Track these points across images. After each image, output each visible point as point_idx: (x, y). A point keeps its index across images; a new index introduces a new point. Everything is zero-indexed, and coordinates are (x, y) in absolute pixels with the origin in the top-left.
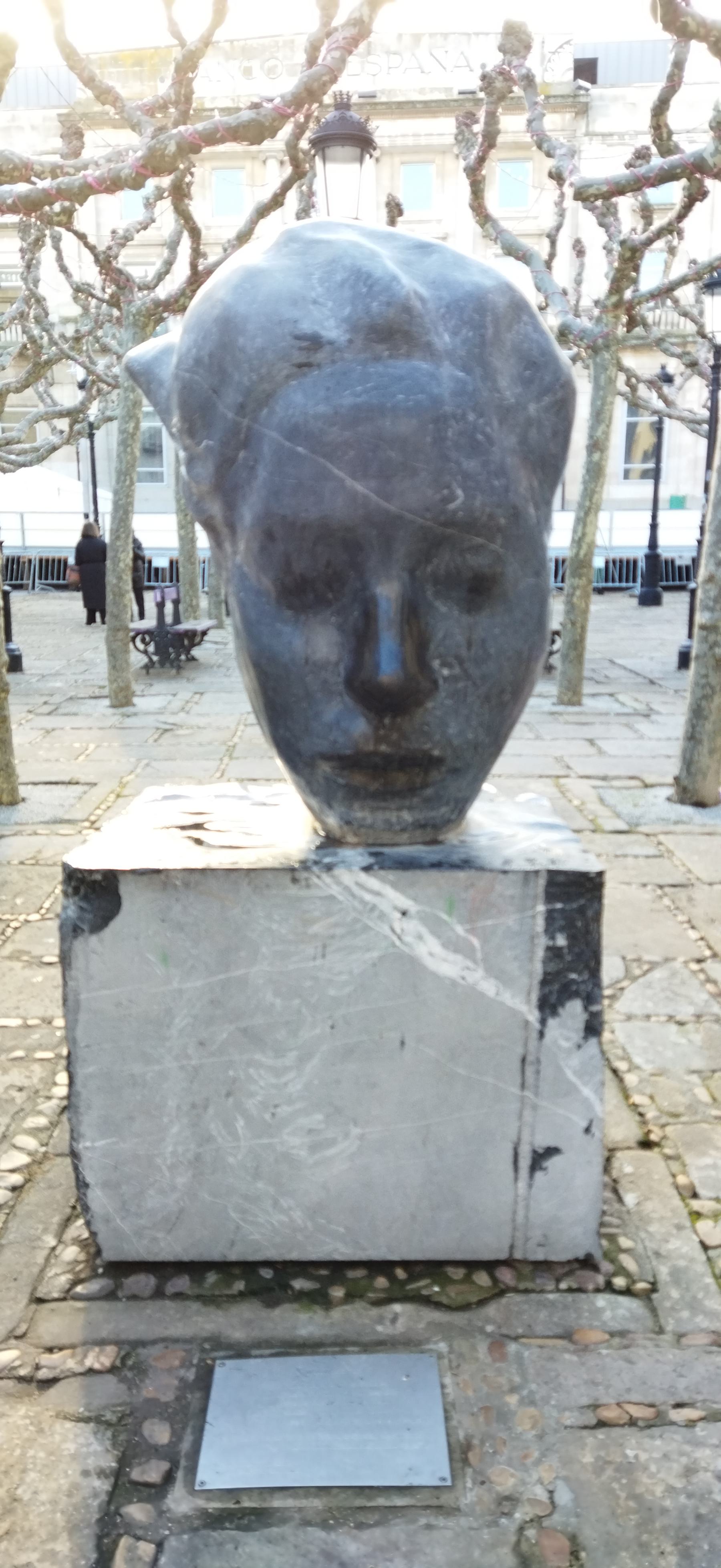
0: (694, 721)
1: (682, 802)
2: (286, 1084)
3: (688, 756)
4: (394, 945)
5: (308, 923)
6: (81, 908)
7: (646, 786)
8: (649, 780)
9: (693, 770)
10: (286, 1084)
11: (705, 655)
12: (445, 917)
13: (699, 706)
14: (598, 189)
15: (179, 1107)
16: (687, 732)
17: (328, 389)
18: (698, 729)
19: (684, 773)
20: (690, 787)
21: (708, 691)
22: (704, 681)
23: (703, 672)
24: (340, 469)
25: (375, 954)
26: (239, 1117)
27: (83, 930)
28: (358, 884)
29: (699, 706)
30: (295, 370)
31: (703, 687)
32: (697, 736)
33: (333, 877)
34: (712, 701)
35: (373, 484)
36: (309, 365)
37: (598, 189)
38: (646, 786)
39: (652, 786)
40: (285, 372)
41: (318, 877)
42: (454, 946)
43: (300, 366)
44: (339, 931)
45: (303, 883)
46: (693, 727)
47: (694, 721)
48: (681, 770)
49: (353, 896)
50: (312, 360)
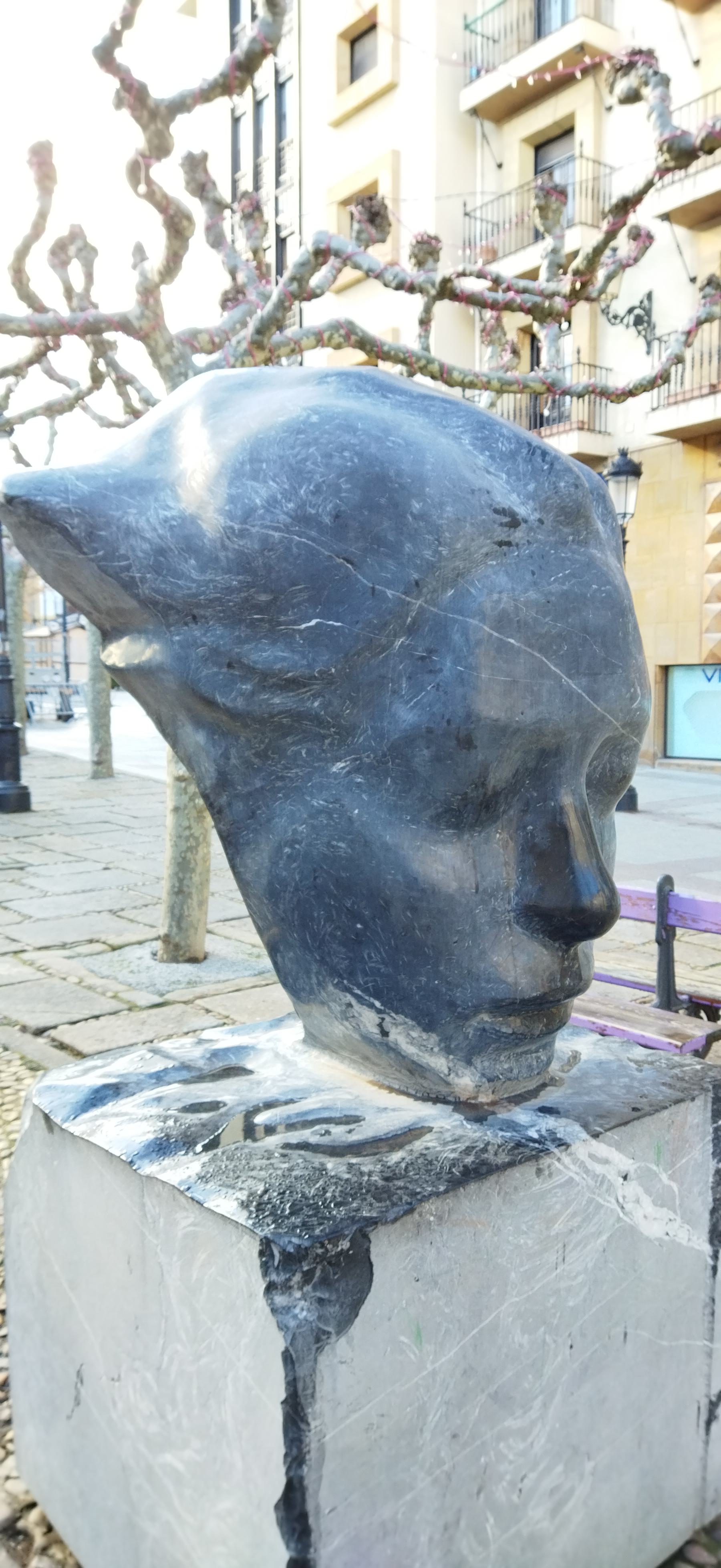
0: (181, 875)
1: (175, 960)
2: (532, 1444)
3: (177, 911)
4: (619, 1219)
5: (550, 1222)
6: (321, 1301)
7: (114, 949)
8: (115, 941)
9: (183, 925)
10: (532, 1444)
11: (186, 807)
12: (655, 1168)
13: (184, 858)
14: (20, 326)
15: (431, 1539)
16: (173, 886)
17: (533, 573)
18: (185, 882)
19: (175, 930)
20: (183, 943)
21: (192, 842)
22: (187, 833)
23: (186, 823)
24: (556, 665)
25: (604, 1237)
26: (489, 1515)
27: (329, 1333)
28: (591, 1156)
29: (184, 858)
30: (496, 547)
31: (187, 839)
32: (185, 889)
33: (570, 1154)
34: (197, 853)
35: (584, 681)
36: (509, 544)
37: (20, 326)
38: (114, 949)
39: (120, 947)
40: (484, 550)
41: (559, 1160)
42: (662, 1200)
43: (501, 544)
44: (576, 1222)
45: (547, 1173)
46: (181, 881)
47: (181, 875)
48: (170, 926)
49: (587, 1171)
50: (511, 539)
